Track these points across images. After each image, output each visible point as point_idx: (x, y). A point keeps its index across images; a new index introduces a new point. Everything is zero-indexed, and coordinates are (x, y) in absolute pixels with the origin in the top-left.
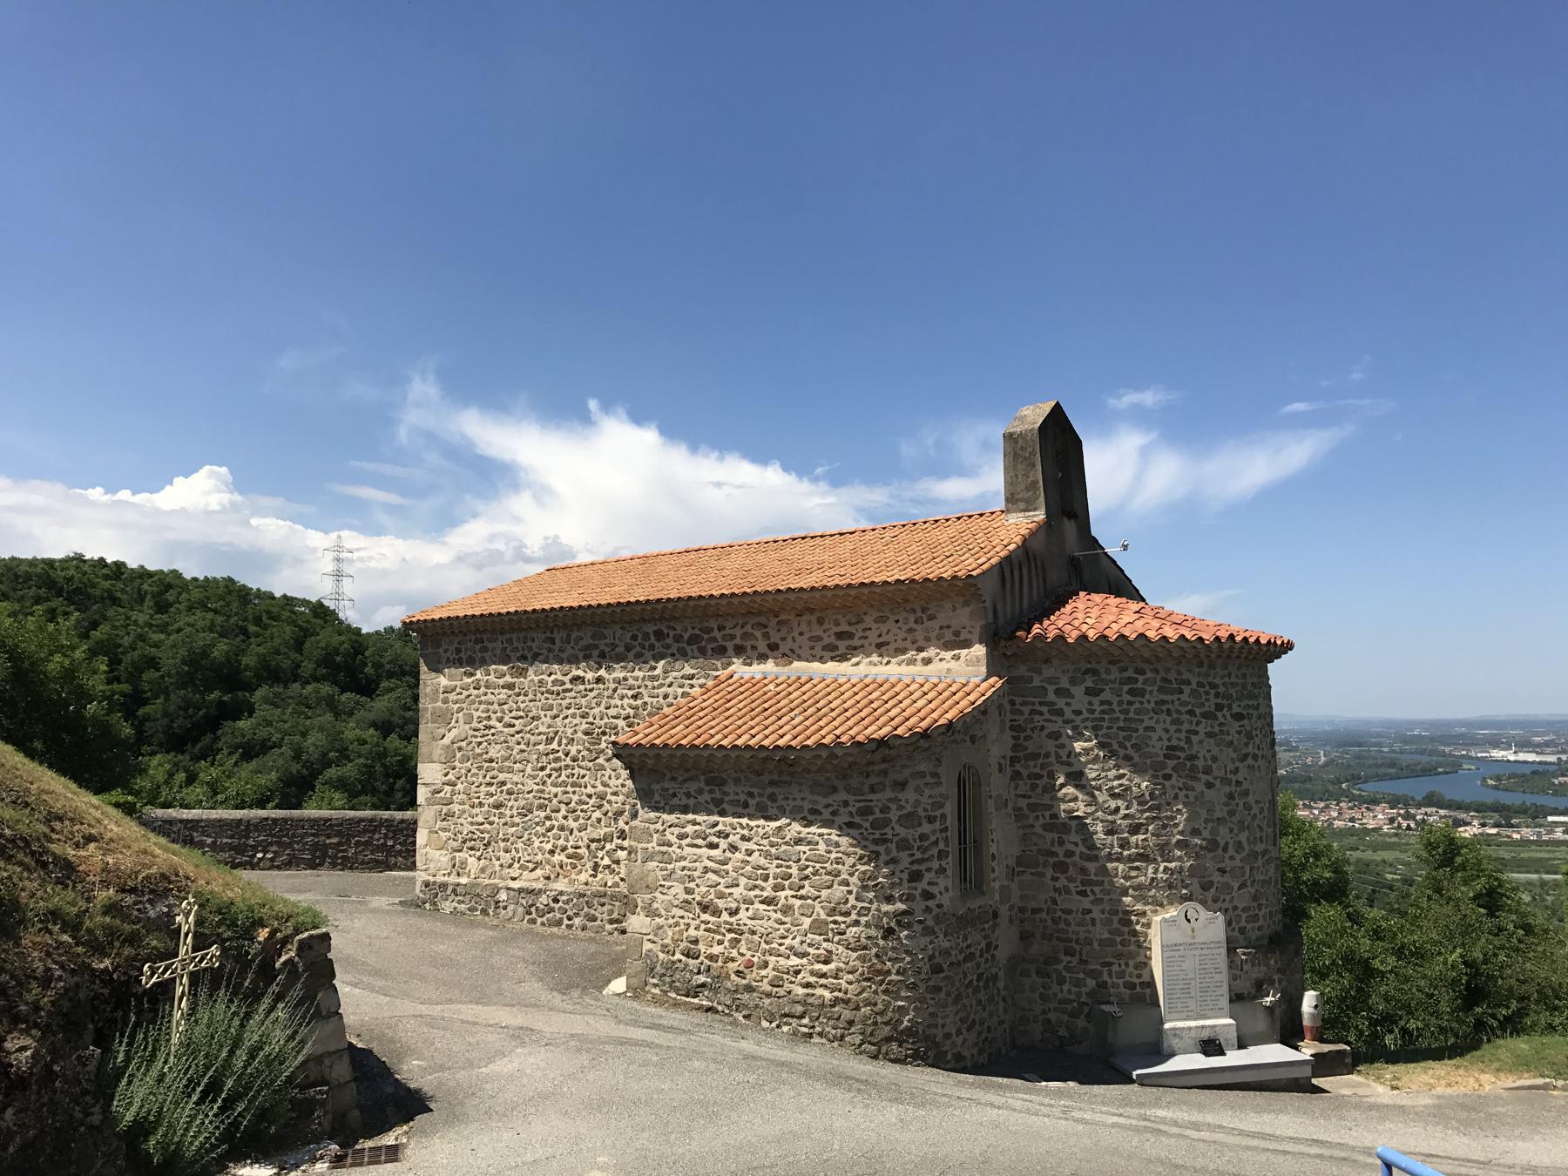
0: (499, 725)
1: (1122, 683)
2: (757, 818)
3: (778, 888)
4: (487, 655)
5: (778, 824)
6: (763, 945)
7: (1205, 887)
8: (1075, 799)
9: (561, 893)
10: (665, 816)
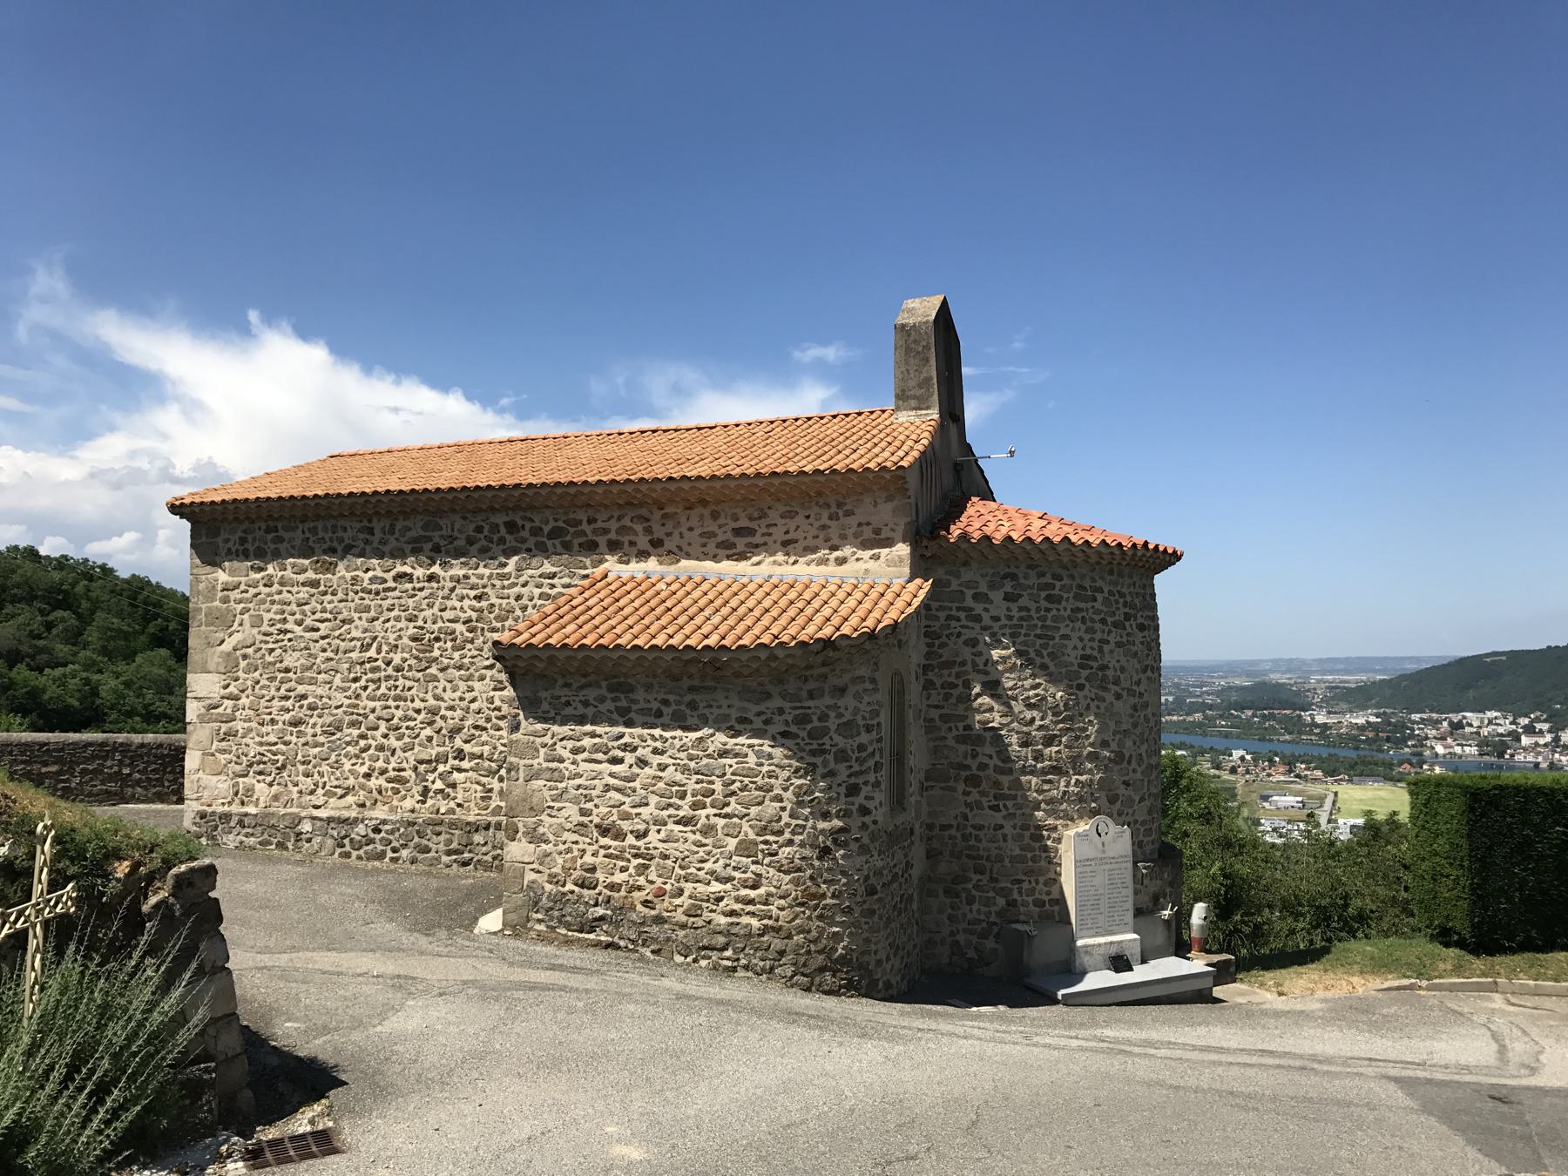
0: (297, 629)
1: (1040, 589)
2: (674, 729)
3: (696, 806)
4: (282, 547)
5: (698, 734)
6: (678, 871)
7: (1112, 800)
8: (991, 710)
9: (384, 822)
10: (555, 728)
